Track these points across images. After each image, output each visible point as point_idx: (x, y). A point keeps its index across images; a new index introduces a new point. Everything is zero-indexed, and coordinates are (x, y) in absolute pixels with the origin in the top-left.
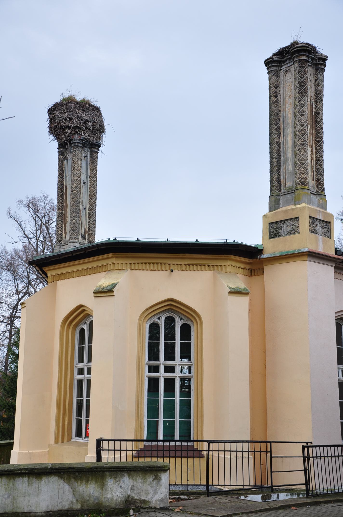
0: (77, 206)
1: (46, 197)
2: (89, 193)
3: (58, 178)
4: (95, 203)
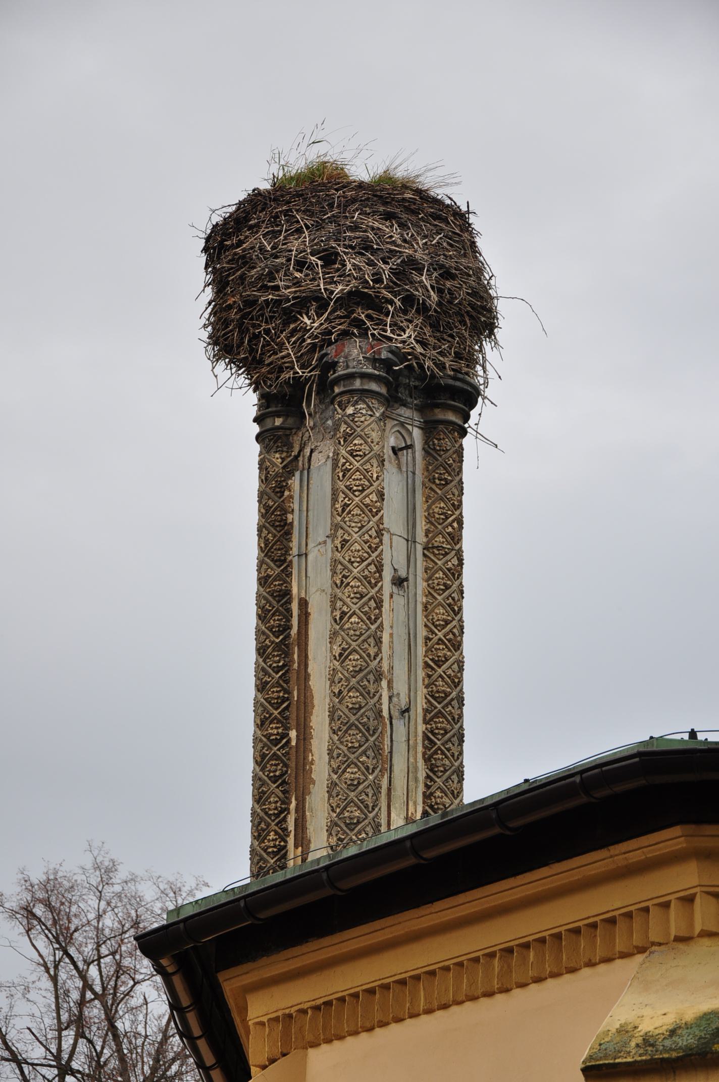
0: (367, 694)
1: (107, 872)
2: (422, 632)
3: (261, 564)
4: (457, 682)
